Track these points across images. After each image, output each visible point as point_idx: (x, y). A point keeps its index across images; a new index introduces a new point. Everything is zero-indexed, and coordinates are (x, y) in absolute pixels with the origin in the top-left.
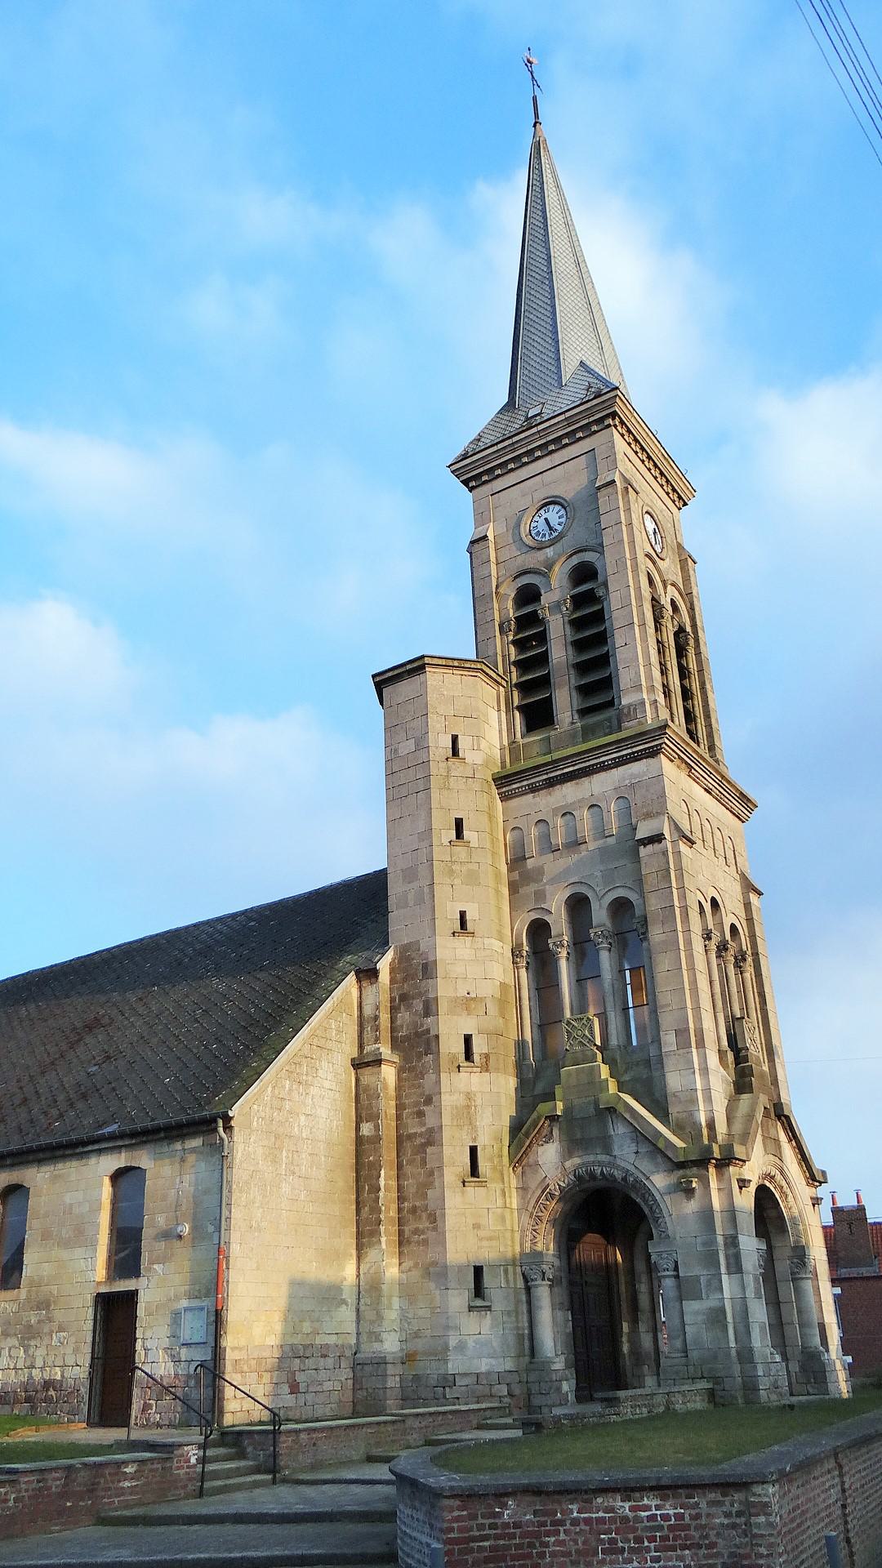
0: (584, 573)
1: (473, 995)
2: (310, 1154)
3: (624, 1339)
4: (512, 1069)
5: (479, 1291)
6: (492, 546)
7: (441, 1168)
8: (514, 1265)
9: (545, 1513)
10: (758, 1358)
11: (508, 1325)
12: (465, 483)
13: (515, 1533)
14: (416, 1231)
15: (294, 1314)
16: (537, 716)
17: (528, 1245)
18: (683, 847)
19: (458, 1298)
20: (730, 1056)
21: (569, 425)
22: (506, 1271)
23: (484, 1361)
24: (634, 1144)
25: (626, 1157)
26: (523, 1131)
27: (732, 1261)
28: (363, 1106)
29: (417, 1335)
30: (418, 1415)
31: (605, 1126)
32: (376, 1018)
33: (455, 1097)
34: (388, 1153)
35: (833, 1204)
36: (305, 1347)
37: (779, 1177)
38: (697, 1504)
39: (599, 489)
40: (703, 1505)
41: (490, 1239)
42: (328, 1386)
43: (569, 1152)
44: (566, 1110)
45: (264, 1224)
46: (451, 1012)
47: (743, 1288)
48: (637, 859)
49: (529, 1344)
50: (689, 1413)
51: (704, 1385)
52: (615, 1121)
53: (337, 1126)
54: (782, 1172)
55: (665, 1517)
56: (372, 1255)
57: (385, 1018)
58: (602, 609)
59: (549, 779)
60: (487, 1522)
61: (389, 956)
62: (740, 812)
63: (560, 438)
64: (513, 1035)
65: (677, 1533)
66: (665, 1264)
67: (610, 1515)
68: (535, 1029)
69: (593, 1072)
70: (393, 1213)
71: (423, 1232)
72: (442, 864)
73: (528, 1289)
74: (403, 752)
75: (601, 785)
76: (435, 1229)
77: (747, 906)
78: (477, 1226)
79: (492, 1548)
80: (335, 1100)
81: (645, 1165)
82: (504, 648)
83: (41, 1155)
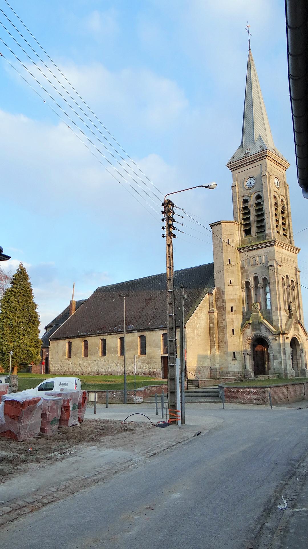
0: (259, 197)
1: (233, 298)
3: (266, 365)
4: (241, 313)
5: (234, 357)
6: (237, 188)
8: (242, 352)
10: (288, 370)
11: (241, 363)
14: (222, 345)
15: (199, 360)
16: (248, 232)
17: (244, 348)
18: (279, 267)
19: (231, 358)
20: (288, 311)
22: (240, 353)
25: (264, 333)
28: (210, 321)
29: (222, 364)
30: (222, 379)
32: (213, 303)
34: (216, 330)
36: (201, 366)
37: (298, 335)
39: (262, 176)
41: (237, 347)
42: (206, 373)
43: (253, 331)
44: (252, 322)
45: (193, 345)
47: (286, 358)
49: (245, 367)
50: (273, 380)
54: (299, 334)
56: (213, 350)
57: (214, 302)
58: (263, 208)
61: (215, 289)
63: (253, 161)
64: (242, 306)
66: (271, 353)
68: (247, 304)
69: (258, 315)
70: (217, 342)
73: (244, 356)
74: (217, 243)
76: (226, 345)
77: (296, 275)
78: (234, 345)
82: (240, 215)
83: (147, 330)
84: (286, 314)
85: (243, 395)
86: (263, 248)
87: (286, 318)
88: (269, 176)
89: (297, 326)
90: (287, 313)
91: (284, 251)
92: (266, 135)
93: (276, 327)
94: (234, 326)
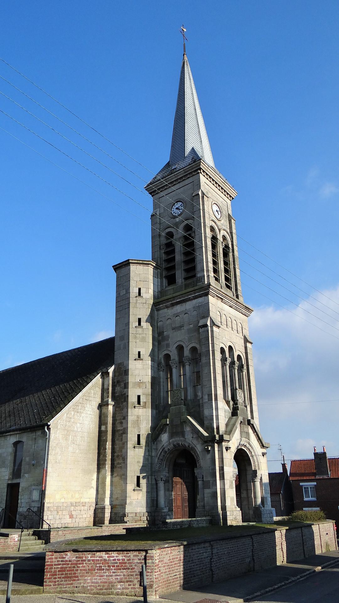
0: (188, 228)
1: (141, 381)
2: (81, 437)
7: (127, 442)
9: (80, 558)
12: (150, 193)
13: (69, 563)
14: (118, 464)
18: (215, 329)
21: (185, 172)
23: (139, 508)
24: (192, 434)
25: (189, 439)
26: (156, 429)
27: (221, 475)
28: (102, 421)
31: (183, 428)
33: (133, 417)
35: (315, 451)
37: (248, 445)
38: (130, 556)
40: (132, 556)
46: (133, 387)
48: (199, 333)
51: (208, 518)
52: (186, 426)
53: (92, 427)
54: (249, 444)
55: (118, 560)
59: (172, 303)
60: (60, 560)
61: (113, 367)
62: (245, 313)
65: (122, 565)
67: (100, 559)
71: (120, 464)
72: (133, 335)
73: (157, 484)
74: (121, 294)
75: (189, 305)
76: (124, 463)
77: (246, 348)
79: (61, 568)
80: (92, 418)
81: (195, 442)
84: (227, 407)
85: (92, 570)
86: (192, 300)
87: (227, 414)
88: (203, 196)
89: (246, 430)
90: (229, 406)
91: (226, 307)
92: (202, 149)
93: (209, 429)
94: (140, 429)
